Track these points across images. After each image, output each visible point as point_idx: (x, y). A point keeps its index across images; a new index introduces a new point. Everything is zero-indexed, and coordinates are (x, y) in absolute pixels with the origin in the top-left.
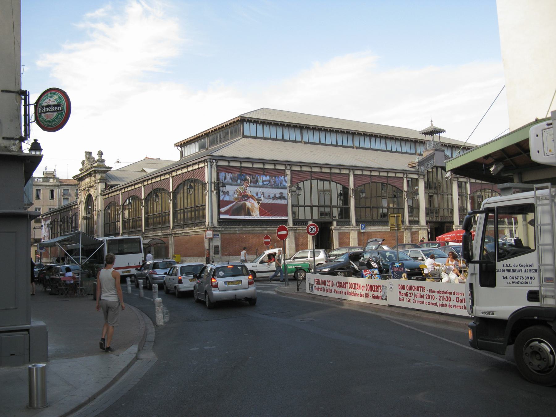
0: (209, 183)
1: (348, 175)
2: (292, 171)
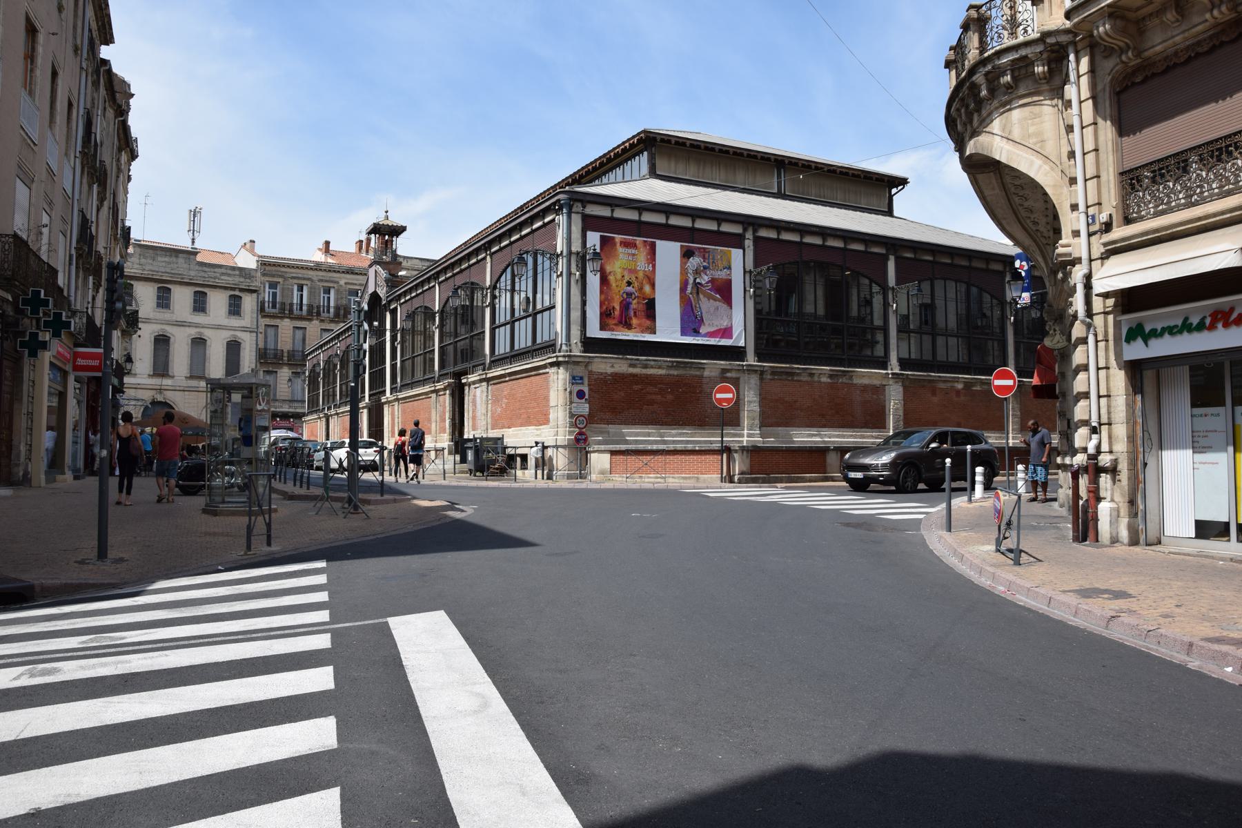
0: (565, 254)
1: (885, 259)
2: (757, 240)
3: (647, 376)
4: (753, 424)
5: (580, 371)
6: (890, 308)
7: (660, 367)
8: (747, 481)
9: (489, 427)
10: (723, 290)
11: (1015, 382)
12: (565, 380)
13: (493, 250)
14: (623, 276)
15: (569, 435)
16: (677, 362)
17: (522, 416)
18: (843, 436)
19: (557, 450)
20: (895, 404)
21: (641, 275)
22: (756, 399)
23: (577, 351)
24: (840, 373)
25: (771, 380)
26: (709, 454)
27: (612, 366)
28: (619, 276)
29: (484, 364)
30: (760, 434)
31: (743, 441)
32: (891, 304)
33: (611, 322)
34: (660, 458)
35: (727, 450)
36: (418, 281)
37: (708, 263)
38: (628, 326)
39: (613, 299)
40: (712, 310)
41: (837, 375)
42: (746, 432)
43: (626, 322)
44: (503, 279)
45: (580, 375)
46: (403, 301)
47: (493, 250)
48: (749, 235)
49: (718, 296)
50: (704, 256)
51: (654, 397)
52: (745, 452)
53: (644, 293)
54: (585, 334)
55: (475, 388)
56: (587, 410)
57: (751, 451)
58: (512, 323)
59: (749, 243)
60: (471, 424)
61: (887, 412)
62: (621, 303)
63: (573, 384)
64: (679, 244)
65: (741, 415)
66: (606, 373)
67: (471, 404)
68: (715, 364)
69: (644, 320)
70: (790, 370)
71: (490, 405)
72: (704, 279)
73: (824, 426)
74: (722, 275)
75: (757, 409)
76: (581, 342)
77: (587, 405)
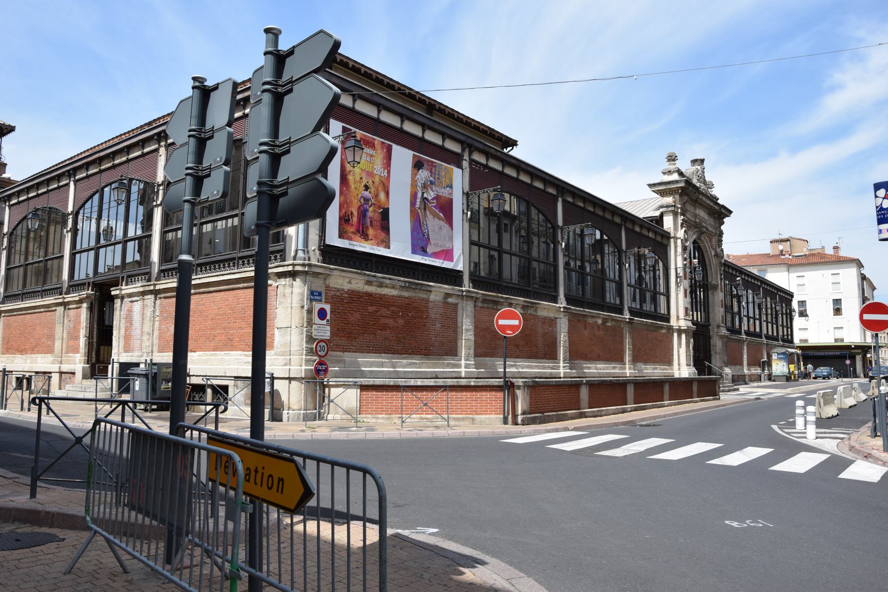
1: (555, 199)
2: (472, 162)
3: (382, 297)
4: (469, 354)
5: (318, 285)
6: (560, 246)
7: (393, 287)
8: (533, 421)
9: (155, 348)
10: (446, 208)
11: (520, 322)
12: (303, 294)
13: (12, 203)
14: (361, 178)
15: (306, 364)
16: (409, 282)
17: (219, 338)
18: (531, 367)
19: (290, 383)
20: (564, 336)
21: (377, 180)
22: (471, 327)
23: (315, 258)
24: (530, 305)
25: (481, 307)
26: (486, 390)
27: (350, 282)
28: (358, 178)
29: (149, 274)
31: (461, 372)
32: (561, 242)
33: (351, 229)
34: (440, 394)
35: (508, 387)
36: (64, 170)
37: (434, 178)
38: (365, 237)
39: (352, 202)
40: (437, 229)
41: (528, 306)
42: (463, 362)
43: (363, 231)
44: (88, 205)
45: (319, 290)
46: (14, 201)
47: (12, 203)
48: (466, 157)
49: (441, 214)
50: (431, 169)
51: (387, 321)
52: (526, 388)
53: (379, 201)
54: (324, 240)
55: (132, 302)
56: (328, 334)
57: (531, 386)
58: (97, 249)
59: (465, 164)
60: (122, 344)
61: (558, 344)
62: (359, 208)
63: (311, 300)
64: (411, 153)
66: (343, 290)
67: (123, 321)
68: (440, 287)
69: (379, 231)
70: (496, 299)
71: (157, 324)
72: (430, 195)
73: (518, 357)
74: (444, 192)
75: (472, 338)
76: (320, 250)
77: (328, 328)
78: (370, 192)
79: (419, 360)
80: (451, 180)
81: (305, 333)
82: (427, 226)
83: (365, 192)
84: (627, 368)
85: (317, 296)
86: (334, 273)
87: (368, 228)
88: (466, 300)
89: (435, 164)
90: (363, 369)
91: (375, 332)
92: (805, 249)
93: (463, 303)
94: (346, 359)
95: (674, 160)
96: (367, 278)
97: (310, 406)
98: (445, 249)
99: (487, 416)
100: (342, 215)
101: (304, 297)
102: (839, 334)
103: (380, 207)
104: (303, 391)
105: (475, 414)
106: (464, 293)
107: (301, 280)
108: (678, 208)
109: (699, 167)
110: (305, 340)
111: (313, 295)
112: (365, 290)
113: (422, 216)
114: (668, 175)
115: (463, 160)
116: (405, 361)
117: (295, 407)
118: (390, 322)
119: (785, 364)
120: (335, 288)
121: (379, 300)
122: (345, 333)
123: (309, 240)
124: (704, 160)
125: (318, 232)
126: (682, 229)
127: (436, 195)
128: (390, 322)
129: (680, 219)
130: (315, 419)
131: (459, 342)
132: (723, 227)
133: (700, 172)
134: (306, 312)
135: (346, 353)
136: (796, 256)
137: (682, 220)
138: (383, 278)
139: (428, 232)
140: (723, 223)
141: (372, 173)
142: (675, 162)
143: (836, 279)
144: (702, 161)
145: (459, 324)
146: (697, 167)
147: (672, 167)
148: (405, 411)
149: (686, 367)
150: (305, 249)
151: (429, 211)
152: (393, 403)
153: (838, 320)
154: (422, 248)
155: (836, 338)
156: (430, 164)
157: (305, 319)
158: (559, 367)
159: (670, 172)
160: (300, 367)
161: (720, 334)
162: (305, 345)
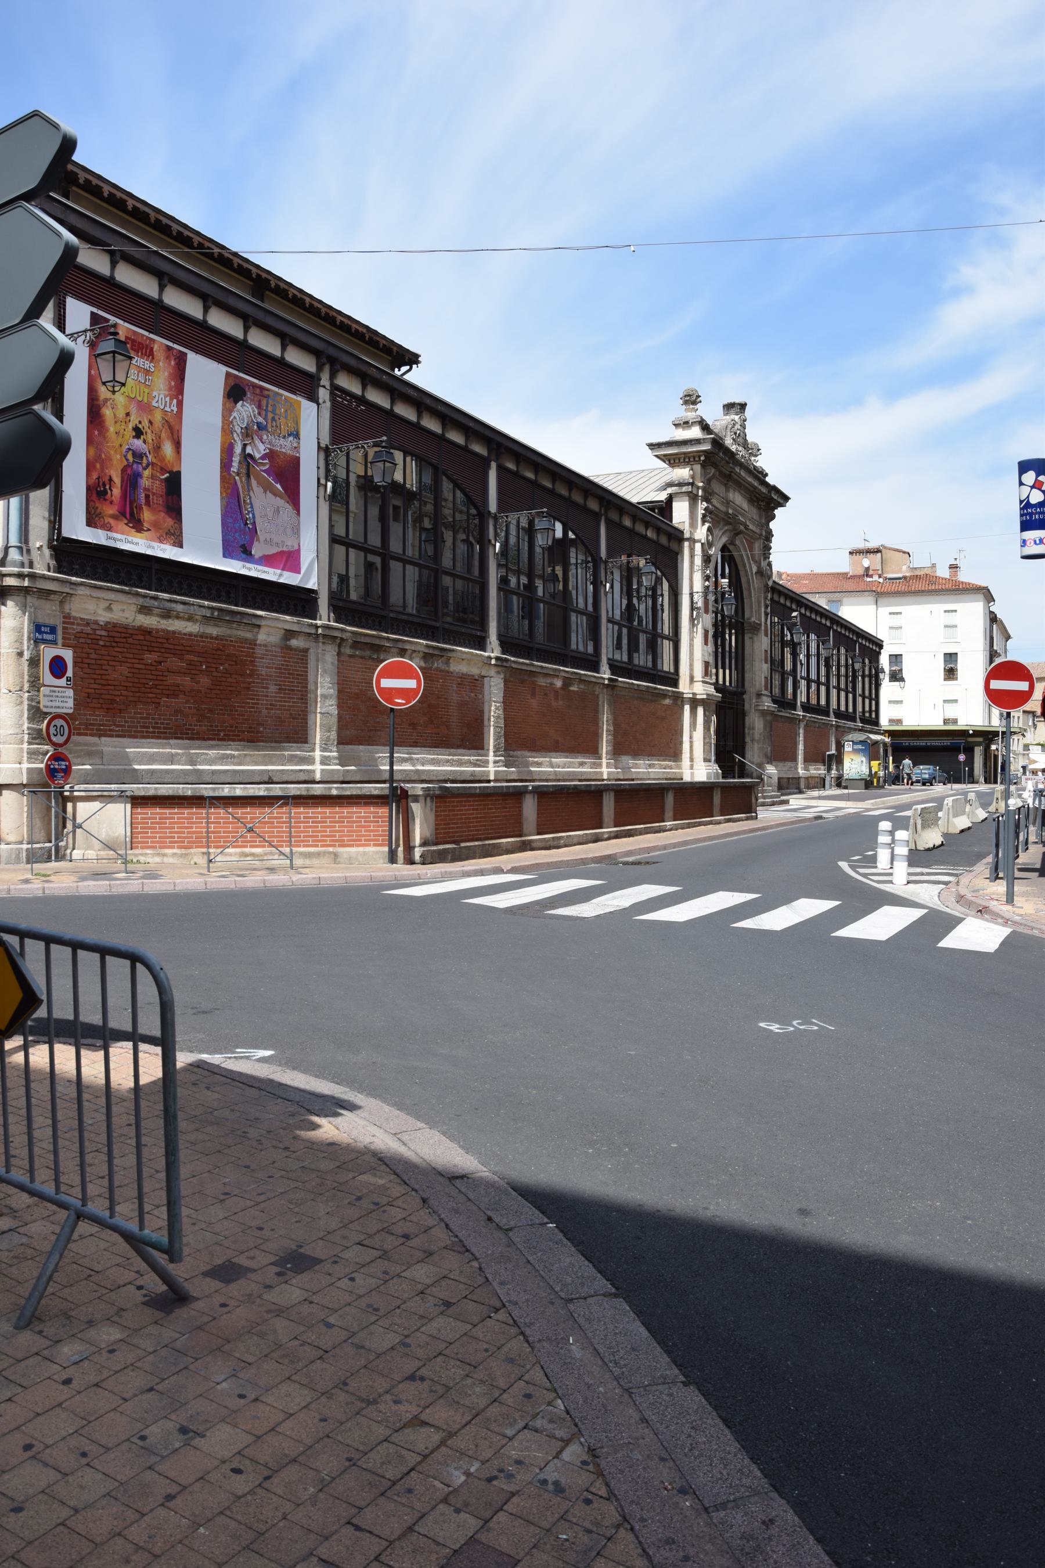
2: (335, 390)
3: (170, 636)
7: (190, 618)
12: (20, 631)
14: (128, 414)
16: (220, 610)
21: (158, 417)
26: (358, 804)
27: (109, 609)
28: (121, 414)
30: (339, 758)
49: (278, 486)
50: (260, 402)
53: (162, 459)
59: (324, 394)
61: (486, 723)
62: (124, 470)
65: (310, 722)
66: (96, 623)
69: (162, 514)
70: (377, 642)
72: (258, 449)
74: (285, 445)
77: (70, 693)
78: (144, 441)
79: (238, 750)
80: (297, 424)
81: (26, 703)
82: (252, 507)
83: (135, 440)
84: (604, 765)
85: (46, 633)
86: (79, 592)
87: (141, 508)
88: (324, 643)
89: (266, 393)
90: (137, 767)
91: (157, 701)
92: (904, 568)
93: (317, 647)
94: (105, 749)
95: (694, 403)
96: (141, 601)
97: (40, 835)
98: (285, 549)
99: (361, 849)
100: (91, 482)
101: (23, 636)
102: (951, 712)
103: (163, 470)
104: (26, 809)
105: (340, 846)
106: (320, 631)
107: (17, 604)
108: (698, 488)
109: (737, 418)
110: (26, 715)
111: (41, 632)
112: (137, 623)
113: (243, 487)
114: (684, 428)
115: (319, 386)
116: (212, 753)
117: (11, 838)
118: (185, 681)
119: (864, 759)
120: (81, 619)
121: (165, 641)
122: (101, 701)
123: (31, 528)
124: (746, 404)
125: (47, 515)
126: (703, 524)
127: (269, 449)
128: (185, 681)
129: (702, 506)
130: (49, 859)
131: (311, 717)
132: (772, 525)
133: (738, 426)
134: (26, 664)
135: (103, 739)
136: (890, 579)
137: (706, 509)
138: (170, 601)
139: (254, 517)
140: (773, 517)
141: (149, 404)
142: (696, 407)
143: (951, 619)
144: (743, 407)
145: (311, 687)
146: (733, 417)
147: (691, 416)
148: (214, 842)
149: (703, 763)
150: (23, 546)
151: (256, 479)
152: (192, 828)
153: (951, 689)
154: (243, 546)
155: (946, 718)
156: (258, 391)
157: (26, 677)
158: (487, 762)
159: (686, 424)
160: (18, 766)
161: (761, 708)
162: (26, 725)
